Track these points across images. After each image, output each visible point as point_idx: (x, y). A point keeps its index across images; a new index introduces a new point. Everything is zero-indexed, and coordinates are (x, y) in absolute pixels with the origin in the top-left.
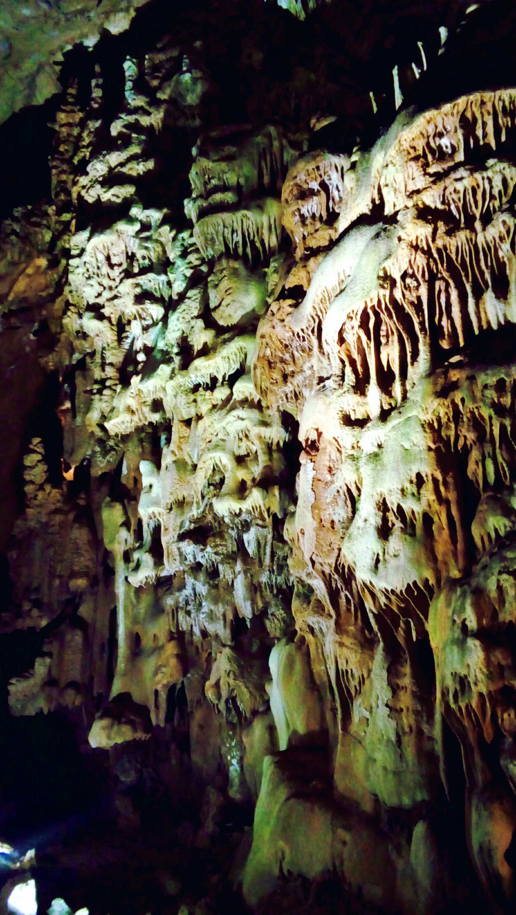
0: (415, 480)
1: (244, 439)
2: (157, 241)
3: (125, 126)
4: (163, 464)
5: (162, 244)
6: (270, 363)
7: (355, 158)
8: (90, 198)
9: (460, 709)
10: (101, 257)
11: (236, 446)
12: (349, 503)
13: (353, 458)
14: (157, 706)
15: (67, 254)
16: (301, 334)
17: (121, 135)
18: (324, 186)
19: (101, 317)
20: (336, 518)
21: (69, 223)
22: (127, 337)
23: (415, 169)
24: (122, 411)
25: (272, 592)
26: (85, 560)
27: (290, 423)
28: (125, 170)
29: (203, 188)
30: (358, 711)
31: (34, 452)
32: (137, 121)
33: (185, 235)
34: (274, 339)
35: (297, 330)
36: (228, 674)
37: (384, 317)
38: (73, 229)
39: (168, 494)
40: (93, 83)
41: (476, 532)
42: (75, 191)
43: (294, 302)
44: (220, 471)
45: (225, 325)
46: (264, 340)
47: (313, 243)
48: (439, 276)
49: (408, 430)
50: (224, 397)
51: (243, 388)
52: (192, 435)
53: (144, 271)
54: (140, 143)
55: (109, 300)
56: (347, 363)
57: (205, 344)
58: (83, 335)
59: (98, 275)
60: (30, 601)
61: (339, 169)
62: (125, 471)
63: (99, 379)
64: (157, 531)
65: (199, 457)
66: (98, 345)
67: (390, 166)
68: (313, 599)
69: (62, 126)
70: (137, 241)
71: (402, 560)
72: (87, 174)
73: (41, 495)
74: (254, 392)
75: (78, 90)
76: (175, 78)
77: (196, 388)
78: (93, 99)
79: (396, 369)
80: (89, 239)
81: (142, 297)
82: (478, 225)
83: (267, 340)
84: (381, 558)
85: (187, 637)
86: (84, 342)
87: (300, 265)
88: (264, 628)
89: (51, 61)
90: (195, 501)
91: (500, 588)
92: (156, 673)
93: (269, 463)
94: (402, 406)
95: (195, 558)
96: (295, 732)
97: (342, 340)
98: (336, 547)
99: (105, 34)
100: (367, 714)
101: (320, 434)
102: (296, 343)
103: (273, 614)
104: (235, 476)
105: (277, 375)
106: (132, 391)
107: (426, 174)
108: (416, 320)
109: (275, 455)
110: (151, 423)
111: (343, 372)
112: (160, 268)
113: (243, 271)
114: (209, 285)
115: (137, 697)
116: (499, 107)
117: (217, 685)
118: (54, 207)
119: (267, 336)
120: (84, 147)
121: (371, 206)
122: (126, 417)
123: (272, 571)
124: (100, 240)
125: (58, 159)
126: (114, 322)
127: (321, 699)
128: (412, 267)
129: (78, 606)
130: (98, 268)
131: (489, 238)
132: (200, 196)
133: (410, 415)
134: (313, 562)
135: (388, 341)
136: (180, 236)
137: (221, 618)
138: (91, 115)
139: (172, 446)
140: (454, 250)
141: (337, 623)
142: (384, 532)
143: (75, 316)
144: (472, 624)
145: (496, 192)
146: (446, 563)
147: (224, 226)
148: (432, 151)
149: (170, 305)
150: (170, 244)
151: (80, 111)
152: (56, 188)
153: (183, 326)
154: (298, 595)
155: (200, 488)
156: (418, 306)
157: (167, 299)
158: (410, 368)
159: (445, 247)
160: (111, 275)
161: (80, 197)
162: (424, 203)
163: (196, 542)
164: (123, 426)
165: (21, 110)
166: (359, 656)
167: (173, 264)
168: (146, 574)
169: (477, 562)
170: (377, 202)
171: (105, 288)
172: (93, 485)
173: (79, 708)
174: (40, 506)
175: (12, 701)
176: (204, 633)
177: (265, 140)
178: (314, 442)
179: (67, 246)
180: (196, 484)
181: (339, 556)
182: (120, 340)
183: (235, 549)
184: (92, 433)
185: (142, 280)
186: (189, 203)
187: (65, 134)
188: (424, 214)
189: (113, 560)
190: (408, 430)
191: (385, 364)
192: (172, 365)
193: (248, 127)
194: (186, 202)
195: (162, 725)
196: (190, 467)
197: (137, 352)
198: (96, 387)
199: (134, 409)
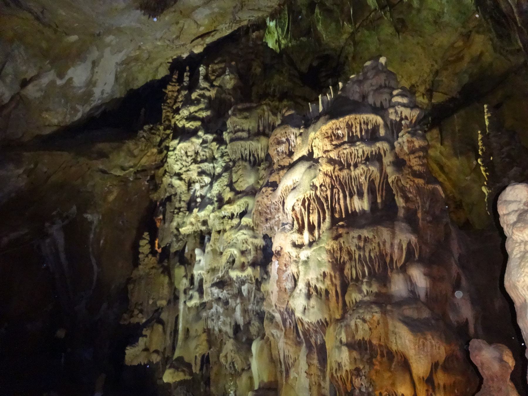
0: (322, 274)
2: (210, 149)
3: (198, 95)
4: (206, 251)
6: (260, 213)
7: (301, 131)
8: (180, 125)
9: (338, 377)
10: (183, 152)
11: (241, 246)
12: (293, 281)
13: (295, 261)
14: (196, 364)
15: (167, 148)
17: (196, 99)
18: (288, 140)
19: (181, 179)
20: (287, 287)
22: (192, 189)
23: (326, 141)
24: (189, 224)
25: (253, 313)
26: (165, 291)
27: (267, 238)
28: (197, 114)
30: (293, 374)
31: (145, 239)
32: (204, 93)
33: (223, 147)
35: (274, 201)
36: (232, 351)
37: (312, 201)
40: (185, 74)
41: (347, 299)
42: (173, 121)
47: (282, 164)
51: (246, 220)
53: (202, 161)
55: (185, 171)
56: (295, 219)
57: (230, 198)
58: (171, 186)
60: (138, 310)
62: (186, 251)
64: (201, 281)
65: (224, 249)
66: (179, 191)
67: (317, 139)
68: (274, 321)
69: (169, 91)
70: (201, 148)
71: (316, 309)
72: (179, 114)
73: (146, 259)
74: (251, 223)
75: (178, 76)
76: (222, 77)
77: (224, 217)
79: (316, 224)
80: (178, 144)
81: (202, 173)
82: (352, 168)
83: (260, 203)
84: (307, 307)
85: (211, 332)
87: (276, 172)
88: (248, 330)
90: (221, 269)
91: (356, 325)
92: (196, 348)
94: (318, 241)
95: (218, 295)
96: (262, 381)
97: (293, 209)
98: (287, 300)
100: (297, 376)
101: (281, 249)
102: (273, 206)
105: (263, 219)
107: (331, 144)
108: (325, 205)
109: (259, 251)
110: (201, 231)
111: (293, 222)
112: (210, 161)
113: (249, 167)
115: (186, 360)
116: (362, 121)
117: (226, 356)
118: (163, 127)
121: (308, 152)
123: (254, 304)
124: (183, 145)
126: (187, 181)
127: (276, 367)
129: (160, 313)
131: (356, 174)
132: (231, 132)
134: (276, 306)
136: (221, 148)
137: (229, 324)
138: (183, 88)
139: (211, 243)
140: (342, 177)
141: (285, 334)
142: (309, 296)
143: (169, 177)
144: (344, 340)
145: (360, 156)
146: (334, 312)
147: (242, 147)
148: (335, 135)
149: (215, 178)
151: (178, 85)
153: (220, 189)
154: (267, 318)
155: (223, 264)
156: (326, 199)
158: (322, 224)
161: (175, 124)
163: (219, 288)
165: (150, 81)
166: (294, 349)
169: (347, 312)
170: (311, 151)
172: (171, 256)
173: (157, 363)
174: (147, 264)
175: (127, 358)
176: (220, 331)
177: (262, 112)
178: (279, 251)
179: (167, 145)
181: (288, 304)
182: (189, 190)
183: (237, 292)
185: (202, 165)
188: (331, 161)
192: (214, 206)
193: (255, 105)
194: (224, 133)
195: (198, 372)
196: (218, 253)
197: (197, 197)
198: (176, 211)
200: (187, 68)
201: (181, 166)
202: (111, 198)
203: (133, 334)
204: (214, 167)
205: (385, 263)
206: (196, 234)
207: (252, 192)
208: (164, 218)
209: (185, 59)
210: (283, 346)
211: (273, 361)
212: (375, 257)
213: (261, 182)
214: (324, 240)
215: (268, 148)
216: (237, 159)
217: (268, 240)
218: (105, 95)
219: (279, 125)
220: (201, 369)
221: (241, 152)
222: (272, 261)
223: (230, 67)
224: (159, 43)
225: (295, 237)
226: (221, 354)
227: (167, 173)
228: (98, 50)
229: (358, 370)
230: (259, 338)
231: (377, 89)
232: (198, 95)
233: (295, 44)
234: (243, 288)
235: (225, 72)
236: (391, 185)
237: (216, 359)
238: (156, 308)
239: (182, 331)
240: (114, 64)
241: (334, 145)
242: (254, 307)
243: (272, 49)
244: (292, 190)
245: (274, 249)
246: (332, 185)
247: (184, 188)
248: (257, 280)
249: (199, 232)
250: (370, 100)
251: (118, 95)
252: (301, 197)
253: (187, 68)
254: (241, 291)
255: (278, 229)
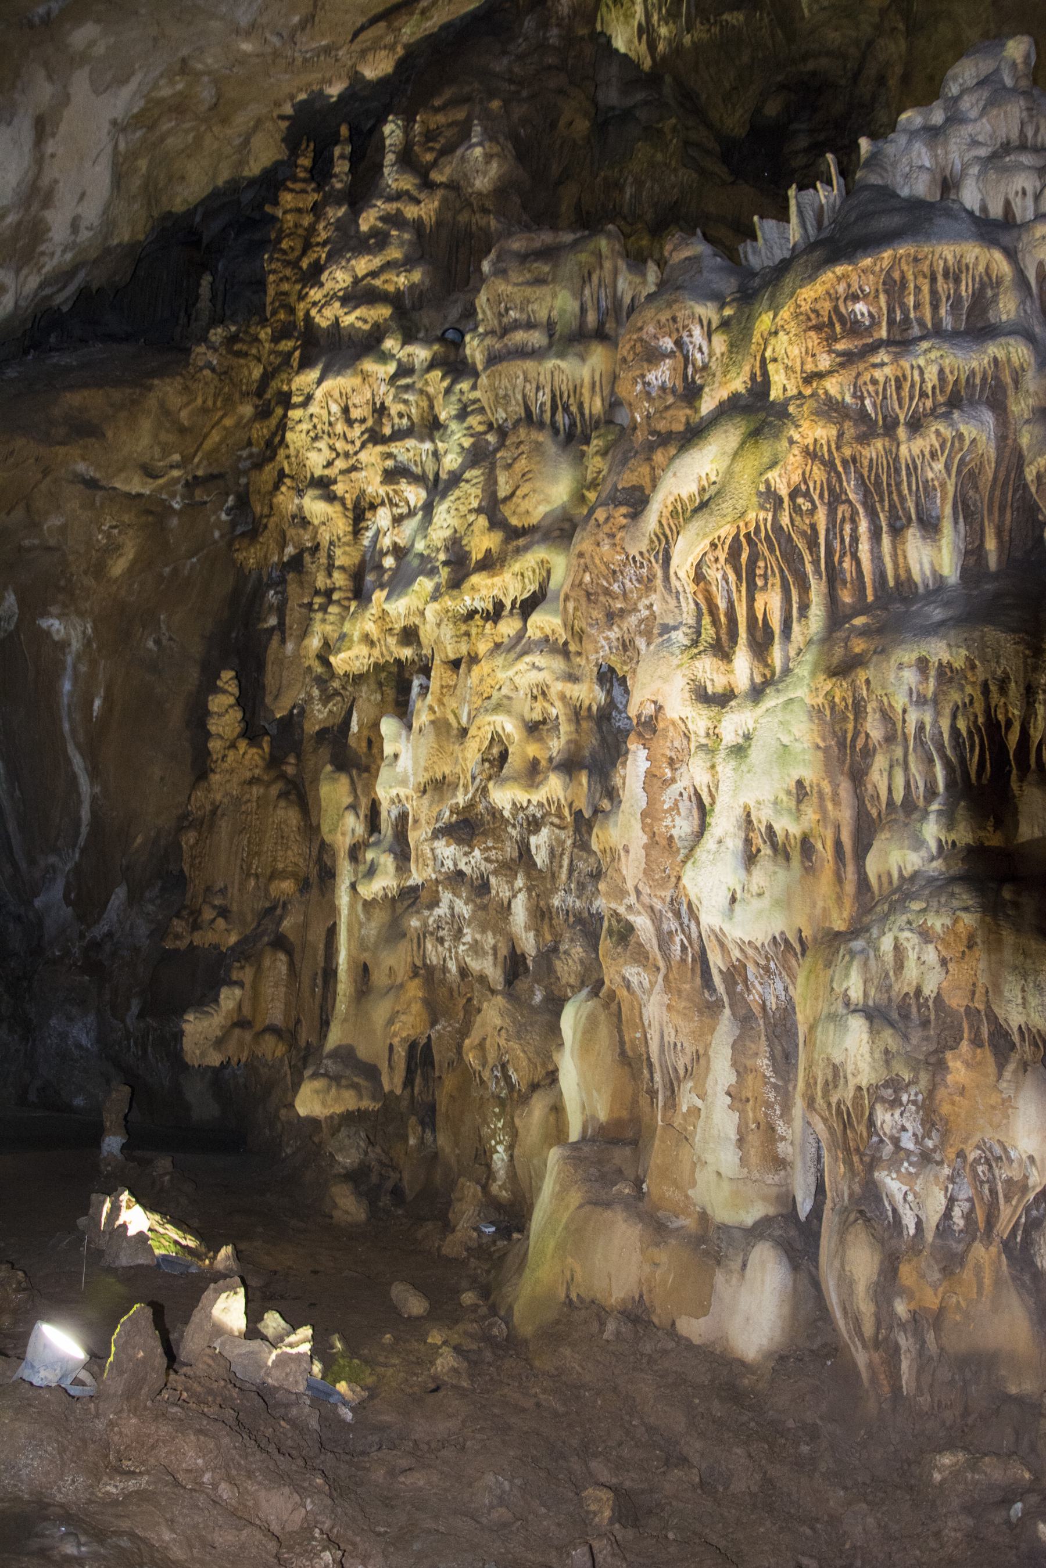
1: (540, 698)
2: (422, 392)
3: (381, 219)
4: (415, 725)
5: (428, 395)
6: (588, 594)
7: (728, 312)
8: (323, 319)
10: (335, 408)
11: (527, 708)
14: (391, 1067)
15: (285, 400)
16: (638, 558)
17: (374, 232)
19: (331, 498)
20: (675, 832)
21: (290, 354)
22: (367, 529)
24: (357, 641)
28: (377, 282)
29: (496, 322)
30: (687, 1099)
31: (225, 692)
33: (465, 385)
34: (597, 561)
35: (633, 552)
37: (763, 548)
38: (295, 364)
39: (421, 770)
40: (337, 151)
43: (631, 510)
44: (501, 741)
45: (520, 525)
46: (582, 561)
47: (662, 426)
48: (844, 497)
49: (788, 717)
50: (512, 633)
51: (545, 622)
52: (460, 684)
53: (398, 435)
54: (402, 244)
55: (342, 472)
57: (489, 551)
58: (302, 521)
59: (329, 435)
60: (214, 907)
61: (705, 323)
62: (354, 727)
63: (323, 589)
65: (471, 719)
67: (781, 333)
68: (632, 940)
70: (393, 390)
72: (322, 285)
73: (231, 755)
75: (315, 161)
76: (459, 152)
77: (471, 614)
78: (336, 176)
79: (776, 624)
80: (320, 382)
82: (902, 432)
84: (738, 896)
85: (438, 975)
86: (301, 531)
88: (551, 970)
89: (275, 115)
92: (391, 1022)
93: (574, 736)
95: (455, 865)
99: (356, 78)
100: (699, 1103)
103: (565, 952)
104: (524, 752)
105: (597, 614)
106: (373, 611)
108: (807, 558)
109: (585, 725)
110: (398, 661)
112: (426, 431)
113: (551, 448)
114: (498, 464)
115: (363, 1053)
117: (481, 1046)
118: (269, 330)
119: (587, 556)
120: (318, 244)
122: (362, 650)
124: (334, 384)
125: (278, 260)
126: (350, 506)
127: (636, 1076)
128: (806, 483)
130: (330, 424)
131: (916, 451)
133: (792, 696)
134: (638, 892)
135: (766, 584)
136: (458, 387)
138: (334, 199)
140: (866, 463)
141: (666, 978)
143: (292, 493)
144: (856, 994)
147: (526, 380)
149: (438, 487)
150: (441, 397)
152: (272, 303)
153: (456, 522)
154: (610, 932)
157: (431, 477)
159: (854, 460)
160: (349, 436)
162: (826, 393)
163: (459, 842)
164: (358, 664)
167: (446, 427)
168: (384, 884)
171: (338, 455)
172: (308, 746)
175: (187, 1044)
179: (285, 388)
180: (465, 759)
181: (676, 886)
182: (357, 532)
183: (516, 854)
184: (309, 668)
185: (395, 448)
186: (472, 339)
187: (291, 224)
188: (831, 410)
189: (334, 857)
190: (788, 717)
191: (760, 617)
192: (436, 579)
195: (398, 1092)
197: (383, 554)
198: (318, 600)
199: (375, 639)
200: (344, 131)
201: (327, 454)
202: (118, 567)
203: (205, 977)
204: (435, 453)
205: (1003, 747)
206: (383, 675)
207: (562, 530)
208: (281, 625)
209: (336, 103)
210: (659, 1014)
211: (631, 1061)
212: (970, 732)
213: (592, 496)
214: (801, 679)
215: (615, 378)
216: (510, 424)
217: (617, 691)
218: (84, 235)
219: (650, 297)
220: (408, 1082)
221: (524, 396)
222: (627, 751)
223: (487, 116)
224: (246, 47)
225: (710, 672)
226: (467, 1042)
227: (287, 481)
228: (50, 78)
229: (895, 1084)
230: (585, 992)
231: (994, 156)
232: (381, 219)
233: (705, 36)
234: (533, 840)
235: (469, 136)
236: (1033, 489)
237: (451, 1055)
238: (267, 905)
239: (349, 968)
240: (106, 127)
241: (839, 354)
242: (570, 900)
243: (626, 55)
244: (696, 511)
245: (632, 712)
246: (831, 490)
247: (342, 526)
248: (578, 815)
249: (394, 669)
250: (970, 196)
251: (124, 235)
252: (726, 531)
253: (344, 131)
254: (529, 850)
255: (648, 644)
